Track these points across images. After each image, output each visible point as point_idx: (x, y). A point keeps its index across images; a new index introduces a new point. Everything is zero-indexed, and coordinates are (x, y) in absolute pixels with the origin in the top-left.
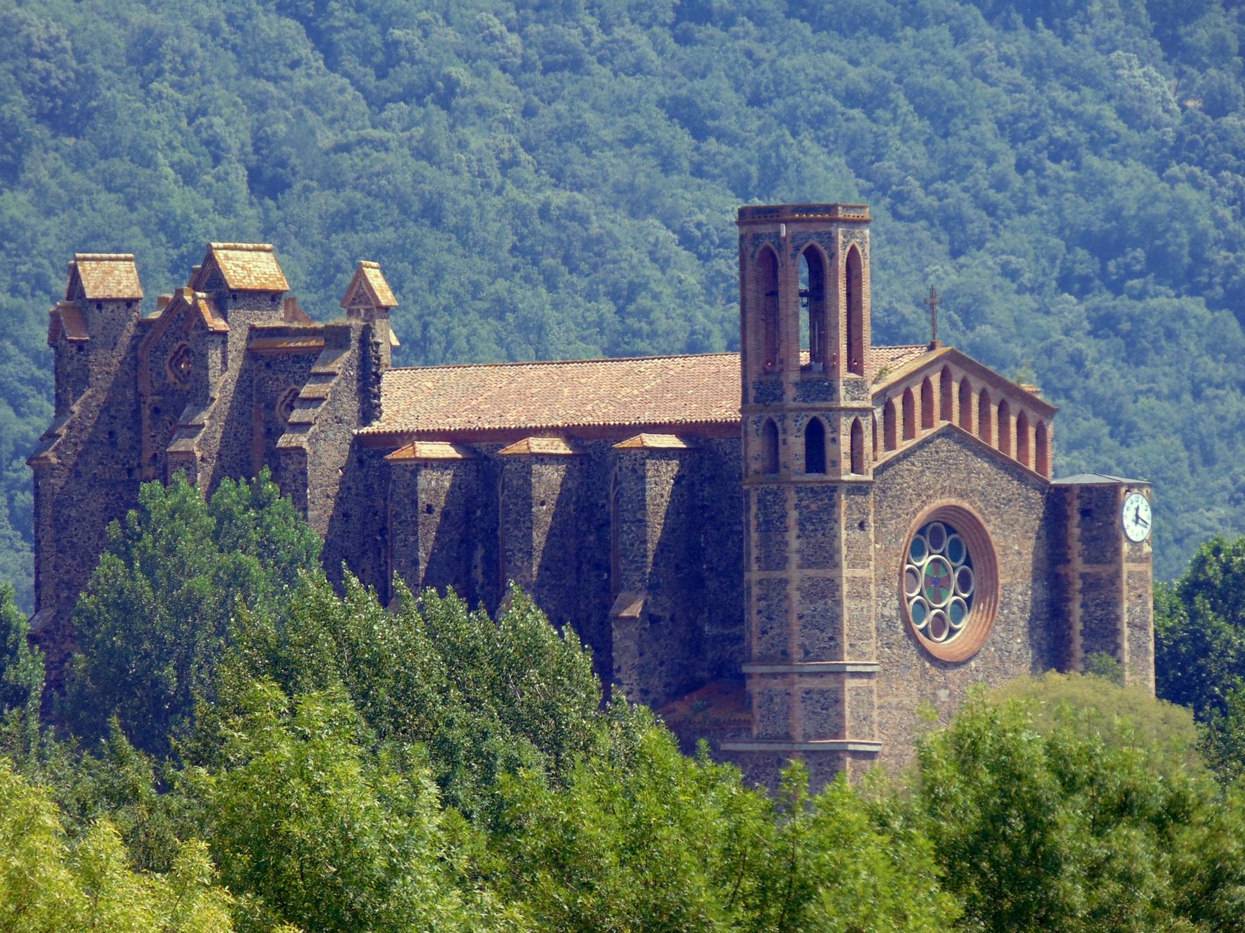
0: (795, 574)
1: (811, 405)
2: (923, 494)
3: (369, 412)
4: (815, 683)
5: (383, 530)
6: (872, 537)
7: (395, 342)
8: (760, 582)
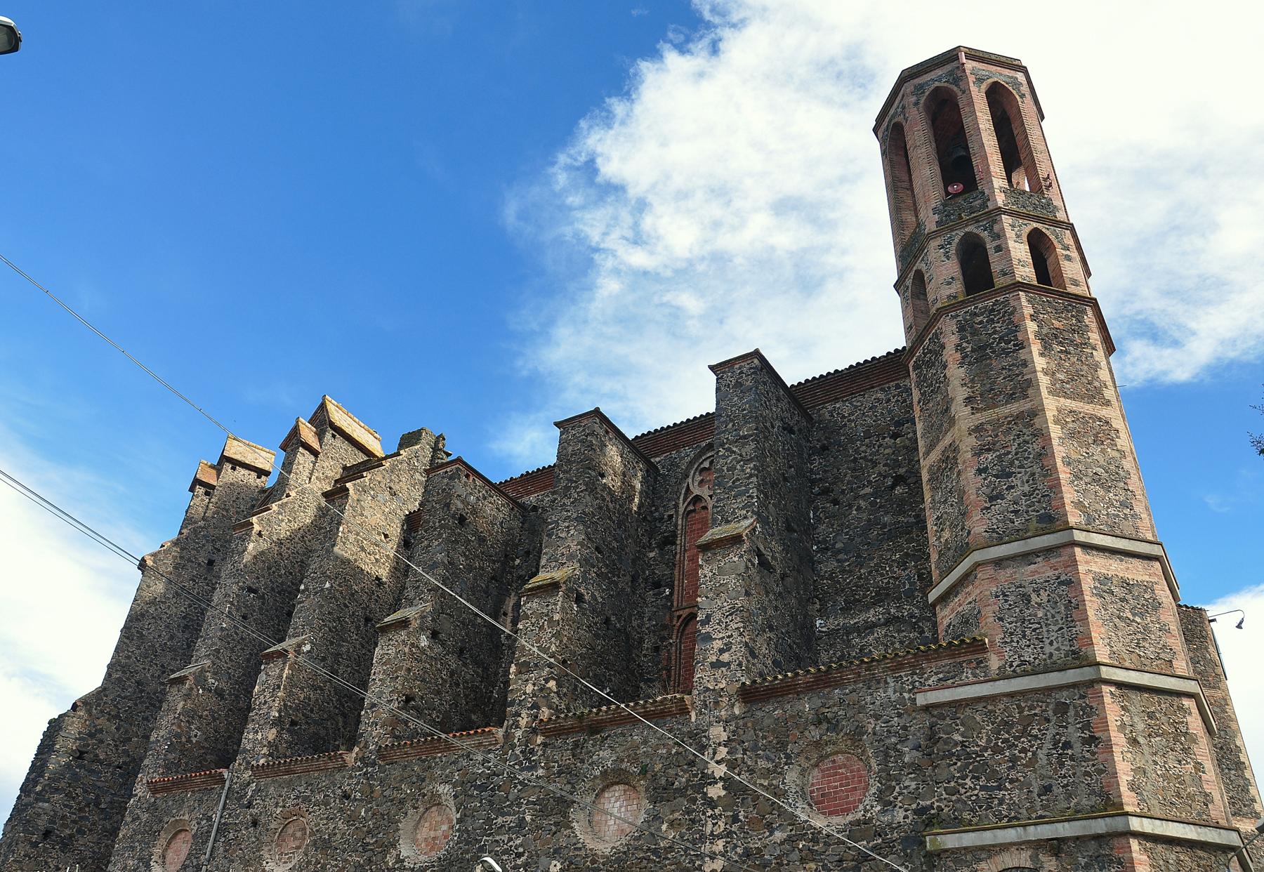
4: (1115, 567)
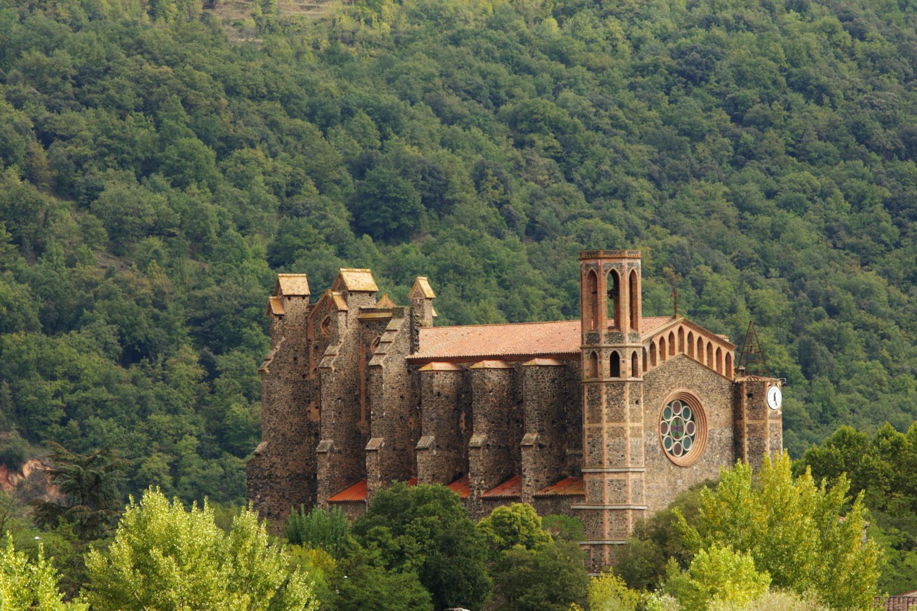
0: (606, 426)
1: (612, 345)
2: (670, 386)
3: (414, 348)
4: (615, 477)
5: (420, 404)
6: (642, 407)
7: (435, 314)
8: (589, 429)
